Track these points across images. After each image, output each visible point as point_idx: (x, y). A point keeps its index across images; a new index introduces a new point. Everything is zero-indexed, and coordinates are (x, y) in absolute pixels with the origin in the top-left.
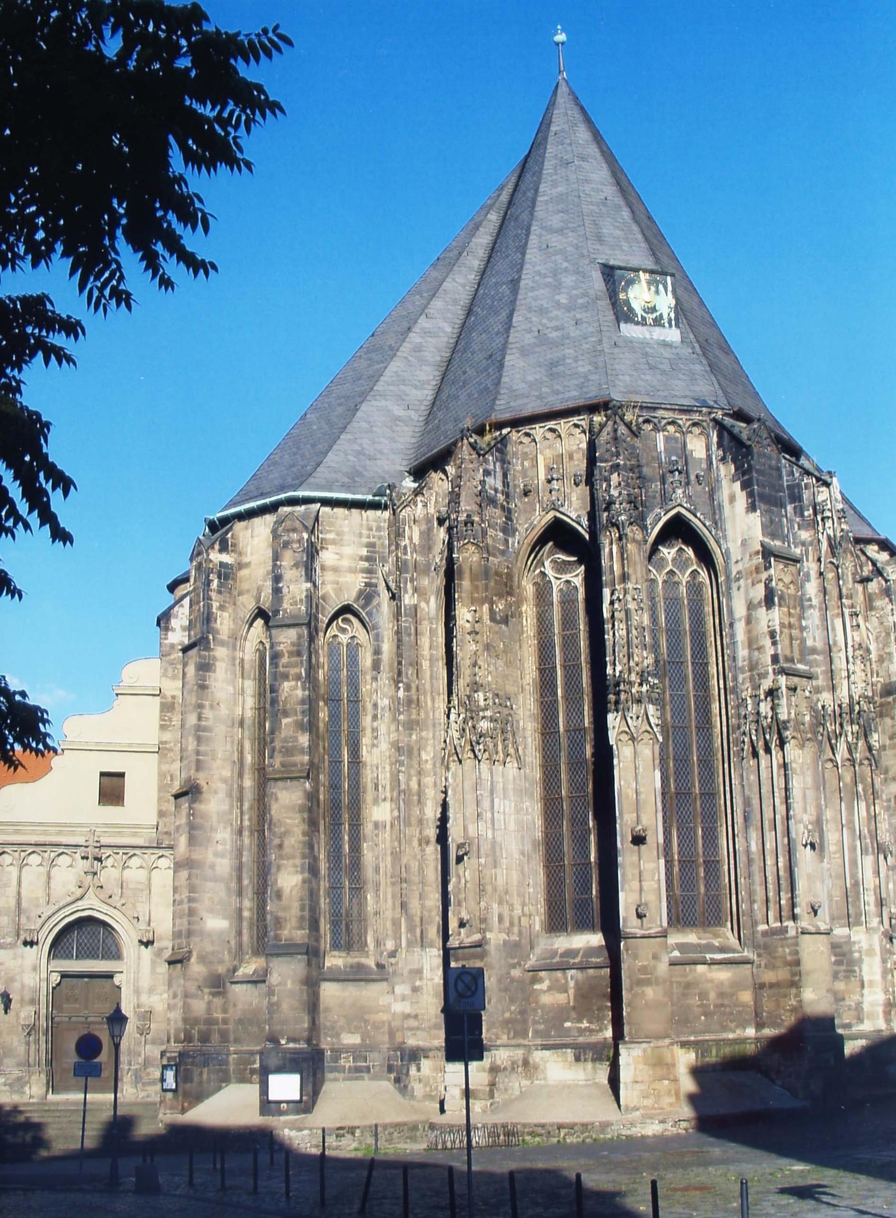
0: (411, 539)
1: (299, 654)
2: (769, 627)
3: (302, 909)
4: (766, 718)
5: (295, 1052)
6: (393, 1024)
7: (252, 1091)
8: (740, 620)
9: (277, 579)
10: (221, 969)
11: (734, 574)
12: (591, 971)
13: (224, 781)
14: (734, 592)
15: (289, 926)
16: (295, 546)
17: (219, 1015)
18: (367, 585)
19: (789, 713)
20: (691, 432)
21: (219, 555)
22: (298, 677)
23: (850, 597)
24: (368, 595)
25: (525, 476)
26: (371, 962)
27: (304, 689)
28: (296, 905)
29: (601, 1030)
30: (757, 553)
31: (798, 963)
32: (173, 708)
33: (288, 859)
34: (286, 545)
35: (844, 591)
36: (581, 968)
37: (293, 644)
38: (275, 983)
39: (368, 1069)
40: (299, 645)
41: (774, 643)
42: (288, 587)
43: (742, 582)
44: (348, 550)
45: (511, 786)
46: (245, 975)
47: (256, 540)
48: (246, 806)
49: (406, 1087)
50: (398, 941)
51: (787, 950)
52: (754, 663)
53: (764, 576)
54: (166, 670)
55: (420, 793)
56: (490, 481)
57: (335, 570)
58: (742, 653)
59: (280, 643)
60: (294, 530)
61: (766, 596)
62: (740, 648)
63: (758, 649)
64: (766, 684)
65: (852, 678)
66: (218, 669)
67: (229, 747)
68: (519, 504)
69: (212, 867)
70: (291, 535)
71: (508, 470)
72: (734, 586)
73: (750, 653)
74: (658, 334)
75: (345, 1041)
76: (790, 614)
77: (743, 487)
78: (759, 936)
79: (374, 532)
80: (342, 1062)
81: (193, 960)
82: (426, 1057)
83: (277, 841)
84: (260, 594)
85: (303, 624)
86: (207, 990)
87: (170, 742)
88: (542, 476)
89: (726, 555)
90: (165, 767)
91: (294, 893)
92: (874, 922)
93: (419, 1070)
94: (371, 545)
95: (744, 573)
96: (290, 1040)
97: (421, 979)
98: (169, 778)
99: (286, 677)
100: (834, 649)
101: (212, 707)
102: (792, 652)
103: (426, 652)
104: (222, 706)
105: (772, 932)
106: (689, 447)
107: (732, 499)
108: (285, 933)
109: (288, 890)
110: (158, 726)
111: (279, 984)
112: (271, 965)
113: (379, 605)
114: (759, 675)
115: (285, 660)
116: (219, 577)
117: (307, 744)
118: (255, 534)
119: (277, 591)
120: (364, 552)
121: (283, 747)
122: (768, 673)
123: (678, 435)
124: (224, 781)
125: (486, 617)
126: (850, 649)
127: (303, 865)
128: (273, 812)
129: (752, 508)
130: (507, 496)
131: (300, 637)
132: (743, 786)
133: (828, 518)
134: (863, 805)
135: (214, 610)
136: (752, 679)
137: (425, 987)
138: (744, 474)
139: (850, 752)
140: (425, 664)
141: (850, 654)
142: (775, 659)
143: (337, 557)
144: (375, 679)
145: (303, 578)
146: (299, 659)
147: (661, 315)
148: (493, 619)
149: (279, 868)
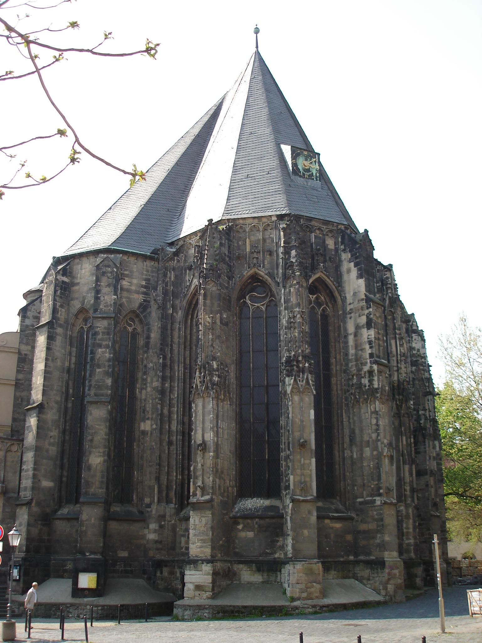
0: (170, 278)
1: (108, 334)
2: (368, 338)
3: (102, 477)
4: (365, 386)
5: (94, 560)
6: (147, 546)
7: (67, 584)
8: (351, 334)
9: (98, 292)
10: (48, 510)
11: (348, 310)
12: (267, 520)
13: (57, 402)
14: (349, 320)
15: (94, 487)
16: (109, 275)
17: (45, 537)
18: (144, 301)
19: (379, 385)
20: (328, 235)
21: (62, 277)
22: (107, 347)
23: (399, 329)
24: (145, 306)
25: (239, 249)
26: (135, 510)
27: (110, 354)
28: (99, 475)
29: (272, 554)
30: (362, 300)
31: (382, 520)
32: (25, 361)
33: (96, 448)
34: (104, 274)
35: (397, 326)
36: (261, 518)
37: (105, 328)
38: (84, 520)
39: (132, 572)
40: (109, 329)
41: (371, 348)
42: (104, 297)
43: (352, 315)
44: (135, 281)
45: (226, 414)
46: (62, 514)
47: (83, 271)
48: (68, 417)
49: (154, 582)
50: (152, 499)
51: (375, 513)
52: (358, 357)
53: (366, 312)
54: (22, 339)
55: (170, 416)
56: (223, 249)
57: (128, 290)
58: (352, 351)
59: (98, 327)
60: (109, 266)
61: (367, 322)
62: (350, 349)
63: (361, 350)
64: (366, 368)
65: (400, 371)
66: (57, 340)
67: (60, 384)
68: (235, 264)
69: (47, 451)
70: (107, 268)
71: (231, 245)
72: (348, 316)
73: (356, 352)
74: (310, 182)
75: (120, 555)
76: (379, 333)
77: (355, 266)
78: (358, 504)
79: (150, 273)
80: (117, 567)
81: (33, 504)
82: (166, 566)
83: (90, 437)
84: (84, 300)
85: (111, 318)
86: (40, 522)
87: (22, 380)
88: (248, 249)
89: (344, 300)
90: (18, 394)
91: (98, 468)
92: (409, 501)
93: (161, 573)
94: (147, 280)
95: (354, 310)
96: (92, 553)
97: (165, 521)
98: (20, 400)
99: (100, 346)
100: (391, 355)
101: (53, 360)
102: (379, 353)
103: (176, 340)
104: (58, 360)
105: (366, 503)
106: (327, 242)
107: (349, 271)
108: (92, 490)
109: (95, 466)
110: (16, 371)
111: (87, 520)
112: (83, 509)
113: (150, 312)
114: (361, 364)
115: (100, 337)
116: (61, 289)
117: (110, 384)
118: (83, 267)
119: (97, 298)
120: (144, 283)
121: (96, 385)
122: (367, 363)
123: (321, 235)
124: (57, 402)
125: (218, 321)
126: (399, 356)
127: (104, 452)
128: (88, 421)
129: (360, 276)
130: (230, 258)
131: (109, 324)
132: (350, 423)
133: (389, 287)
134: (404, 438)
135: (57, 307)
136: (357, 365)
137: (166, 525)
138: (356, 258)
139: (397, 408)
140: (175, 347)
141: (399, 358)
142: (371, 355)
143: (129, 284)
144: (146, 352)
145: (113, 293)
146: (108, 336)
147: (312, 173)
148: (221, 323)
149: (90, 453)
